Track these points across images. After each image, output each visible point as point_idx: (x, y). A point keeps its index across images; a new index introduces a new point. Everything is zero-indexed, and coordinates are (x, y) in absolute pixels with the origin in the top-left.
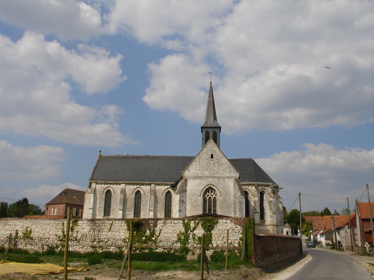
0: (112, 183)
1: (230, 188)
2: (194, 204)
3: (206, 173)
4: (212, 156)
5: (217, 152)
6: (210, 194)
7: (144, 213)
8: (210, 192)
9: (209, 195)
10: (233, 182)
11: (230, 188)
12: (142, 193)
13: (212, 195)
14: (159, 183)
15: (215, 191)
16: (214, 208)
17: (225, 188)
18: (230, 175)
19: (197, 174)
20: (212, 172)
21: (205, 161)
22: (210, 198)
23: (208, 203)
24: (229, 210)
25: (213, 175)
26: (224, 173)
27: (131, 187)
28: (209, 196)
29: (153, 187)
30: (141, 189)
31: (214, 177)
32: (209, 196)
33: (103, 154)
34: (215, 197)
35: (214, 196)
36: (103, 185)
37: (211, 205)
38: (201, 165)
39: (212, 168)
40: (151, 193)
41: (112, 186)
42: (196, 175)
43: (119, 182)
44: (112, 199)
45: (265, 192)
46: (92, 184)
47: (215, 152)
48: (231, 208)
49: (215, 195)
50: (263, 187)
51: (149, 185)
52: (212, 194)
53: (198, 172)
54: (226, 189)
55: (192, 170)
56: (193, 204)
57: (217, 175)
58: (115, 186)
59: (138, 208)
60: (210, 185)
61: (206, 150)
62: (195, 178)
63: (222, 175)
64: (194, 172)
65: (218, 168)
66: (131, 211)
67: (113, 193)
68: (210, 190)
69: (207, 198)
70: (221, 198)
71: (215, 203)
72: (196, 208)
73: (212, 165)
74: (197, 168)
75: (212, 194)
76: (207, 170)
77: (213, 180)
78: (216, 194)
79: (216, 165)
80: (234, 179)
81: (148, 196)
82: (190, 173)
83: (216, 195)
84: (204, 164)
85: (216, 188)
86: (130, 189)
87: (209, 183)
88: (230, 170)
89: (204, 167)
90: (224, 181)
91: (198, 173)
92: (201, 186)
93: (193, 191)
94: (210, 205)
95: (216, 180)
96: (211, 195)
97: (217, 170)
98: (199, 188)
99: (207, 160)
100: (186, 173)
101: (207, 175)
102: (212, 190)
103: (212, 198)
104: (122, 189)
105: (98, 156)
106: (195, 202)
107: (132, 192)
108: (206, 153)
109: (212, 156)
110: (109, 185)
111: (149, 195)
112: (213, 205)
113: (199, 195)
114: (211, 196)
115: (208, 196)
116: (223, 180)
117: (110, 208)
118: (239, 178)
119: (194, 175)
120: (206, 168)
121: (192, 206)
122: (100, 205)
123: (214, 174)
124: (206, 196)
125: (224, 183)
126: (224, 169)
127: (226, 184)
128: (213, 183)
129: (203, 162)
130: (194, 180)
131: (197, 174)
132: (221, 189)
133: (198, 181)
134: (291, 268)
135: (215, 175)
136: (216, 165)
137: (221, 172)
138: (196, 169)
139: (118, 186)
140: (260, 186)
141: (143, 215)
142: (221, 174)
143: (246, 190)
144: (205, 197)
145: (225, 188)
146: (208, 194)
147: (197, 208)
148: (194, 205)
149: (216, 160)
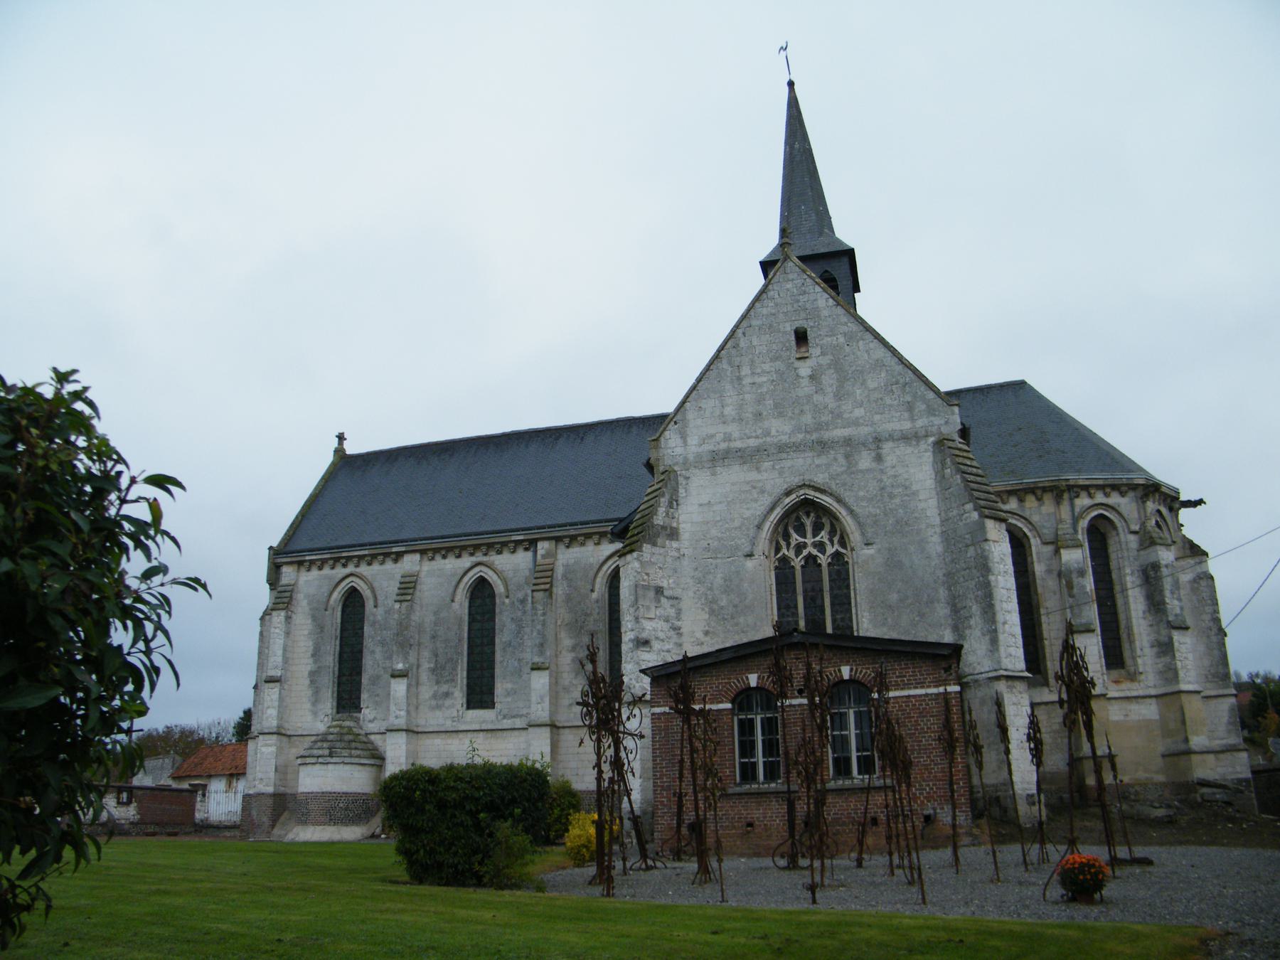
0: (365, 556)
1: (915, 493)
2: (723, 603)
3: (780, 429)
4: (801, 337)
5: (825, 313)
6: (809, 540)
7: (509, 686)
8: (809, 529)
9: (805, 545)
10: (928, 457)
11: (915, 493)
12: (499, 588)
13: (821, 546)
14: (573, 532)
15: (837, 519)
16: (838, 617)
17: (891, 496)
18: (907, 425)
19: (728, 438)
20: (808, 419)
21: (766, 367)
22: (811, 559)
23: (805, 591)
24: (922, 615)
25: (815, 436)
26: (877, 417)
27: (449, 566)
28: (805, 553)
29: (543, 557)
30: (491, 573)
31: (823, 446)
32: (805, 553)
33: (351, 448)
34: (837, 555)
35: (830, 550)
36: (327, 571)
37: (818, 602)
38: (748, 388)
39: (809, 397)
40: (548, 580)
41: (364, 569)
42: (723, 446)
43: (394, 550)
44: (367, 629)
45: (1115, 528)
46: (285, 569)
47: (814, 313)
48: (932, 602)
49: (836, 540)
50: (1100, 498)
51: (526, 549)
52: (818, 539)
53: (733, 429)
54: (897, 501)
55: (699, 422)
56: (714, 601)
57: (839, 433)
58: (376, 567)
59: (485, 665)
60: (800, 487)
61: (765, 311)
62: (718, 459)
63: (864, 430)
64: (711, 431)
65: (838, 397)
66: (453, 680)
67: (369, 604)
68: (808, 516)
69: (797, 563)
70: (870, 551)
71: (840, 588)
72: (737, 624)
73: (805, 382)
74: (729, 411)
75: (823, 536)
76: (781, 415)
77: (817, 462)
78: (842, 537)
79: (829, 379)
80: (931, 439)
81: (523, 601)
82: (693, 441)
83: (843, 543)
84: (760, 385)
85: (839, 500)
86: (441, 579)
87: (797, 480)
88: (908, 398)
89: (760, 400)
90: (879, 458)
91: (736, 435)
92: (756, 501)
93: (714, 532)
94: (813, 599)
95: (835, 459)
96: (815, 545)
97: (832, 404)
98: (747, 514)
99: (778, 363)
100: (672, 443)
101: (785, 438)
102: (818, 517)
103: (824, 560)
104: (407, 579)
105: (327, 459)
106: (727, 590)
107: (451, 590)
108: (771, 326)
109: (801, 337)
110: (351, 568)
111: (529, 592)
112: (834, 598)
113: (747, 550)
114: (815, 552)
115: (800, 548)
116: (873, 454)
117: (359, 673)
118: (964, 433)
119: (711, 447)
120: (776, 406)
121: (712, 612)
122: (315, 662)
123: (819, 427)
124: (791, 554)
125: (882, 471)
126: (876, 395)
127: (891, 472)
128: (820, 478)
129: (753, 373)
130: (714, 474)
131: (728, 438)
132: (864, 504)
133: (735, 475)
134: (501, 613)
135: (827, 435)
136: (829, 379)
137: (859, 412)
138: (722, 415)
139: (389, 565)
140: (1084, 494)
141: (508, 694)
142: (856, 423)
143: (1020, 524)
144: (784, 561)
145: (891, 496)
146: (795, 538)
147: (741, 620)
148: (722, 608)
149: (823, 354)
